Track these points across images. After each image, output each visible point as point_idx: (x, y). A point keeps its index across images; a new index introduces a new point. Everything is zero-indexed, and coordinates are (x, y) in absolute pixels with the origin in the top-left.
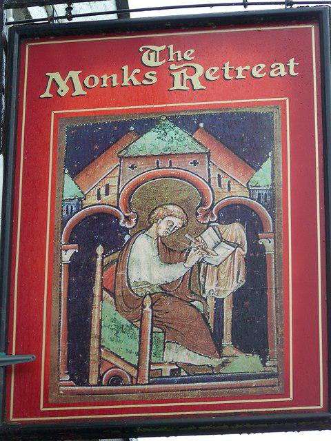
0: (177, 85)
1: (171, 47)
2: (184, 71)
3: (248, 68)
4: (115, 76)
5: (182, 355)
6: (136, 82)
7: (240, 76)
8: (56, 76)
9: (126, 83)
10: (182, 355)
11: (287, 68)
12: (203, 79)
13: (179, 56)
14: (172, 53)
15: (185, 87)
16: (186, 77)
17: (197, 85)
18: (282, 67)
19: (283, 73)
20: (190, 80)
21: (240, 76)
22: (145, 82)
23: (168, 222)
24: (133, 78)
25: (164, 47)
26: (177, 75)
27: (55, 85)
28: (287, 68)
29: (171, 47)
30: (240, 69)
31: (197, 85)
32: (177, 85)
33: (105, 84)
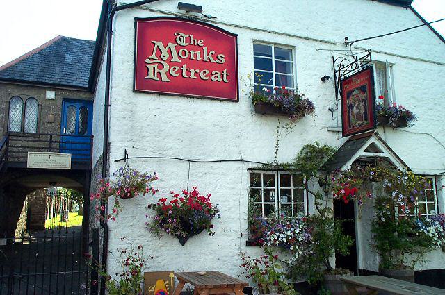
0: (151, 76)
1: (192, 36)
2: (156, 66)
3: (197, 71)
4: (199, 53)
5: (359, 122)
6: (212, 60)
7: (192, 76)
8: (159, 44)
9: (206, 59)
10: (359, 122)
11: (222, 76)
12: (169, 74)
13: (196, 42)
14: (192, 41)
15: (156, 78)
16: (157, 70)
17: (165, 78)
18: (219, 74)
19: (220, 79)
20: (159, 73)
21: (192, 76)
22: (217, 61)
23: (357, 103)
24: (210, 56)
25: (188, 36)
26: (151, 68)
27: (159, 51)
28: (222, 76)
29: (192, 36)
30: (193, 71)
31: (165, 78)
32: (151, 76)
33: (192, 57)
